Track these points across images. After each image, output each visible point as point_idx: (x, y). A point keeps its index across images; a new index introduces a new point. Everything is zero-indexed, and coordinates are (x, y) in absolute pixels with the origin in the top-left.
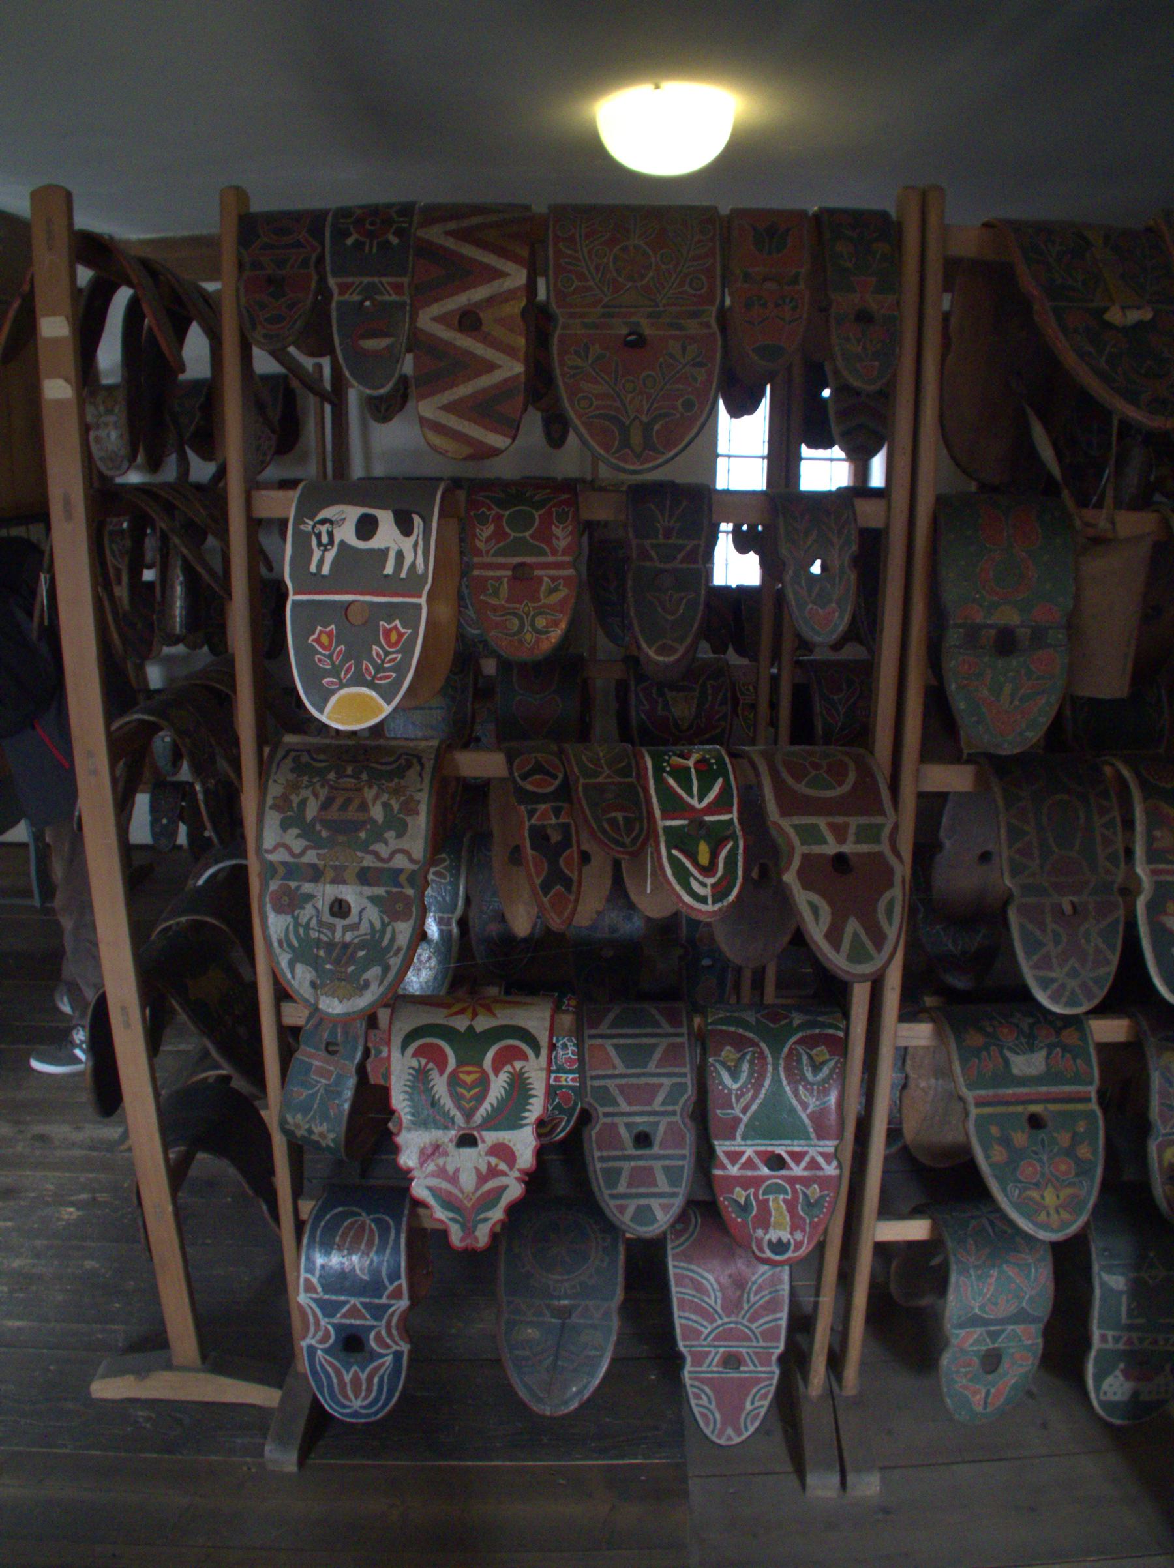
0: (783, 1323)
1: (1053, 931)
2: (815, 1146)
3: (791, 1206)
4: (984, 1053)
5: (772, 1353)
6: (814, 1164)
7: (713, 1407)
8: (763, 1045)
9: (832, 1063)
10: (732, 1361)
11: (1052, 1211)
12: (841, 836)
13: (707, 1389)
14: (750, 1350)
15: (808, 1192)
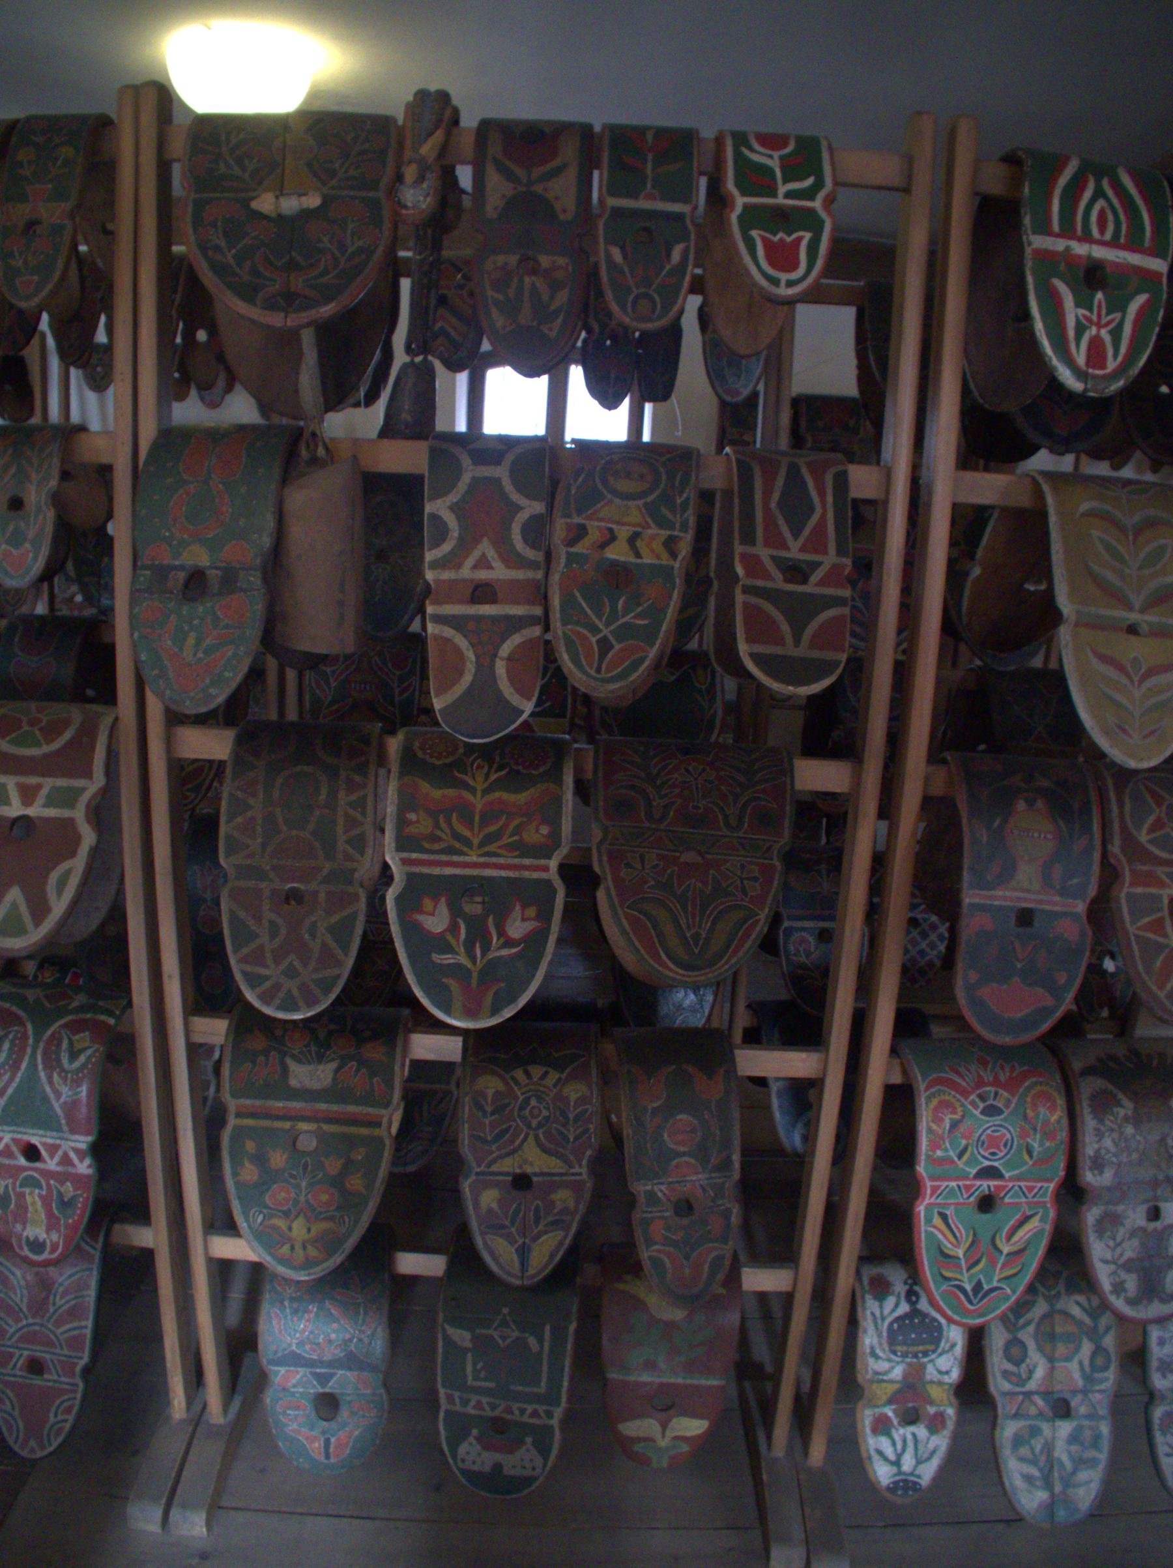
0: (88, 1332)
1: (271, 922)
2: (67, 1140)
3: (46, 1201)
4: (262, 1058)
5: (76, 1364)
6: (66, 1161)
7: (16, 1413)
8: (29, 1027)
9: (89, 1052)
10: (36, 1367)
11: (298, 1246)
12: (27, 799)
13: (9, 1392)
14: (54, 1357)
15: (62, 1190)
